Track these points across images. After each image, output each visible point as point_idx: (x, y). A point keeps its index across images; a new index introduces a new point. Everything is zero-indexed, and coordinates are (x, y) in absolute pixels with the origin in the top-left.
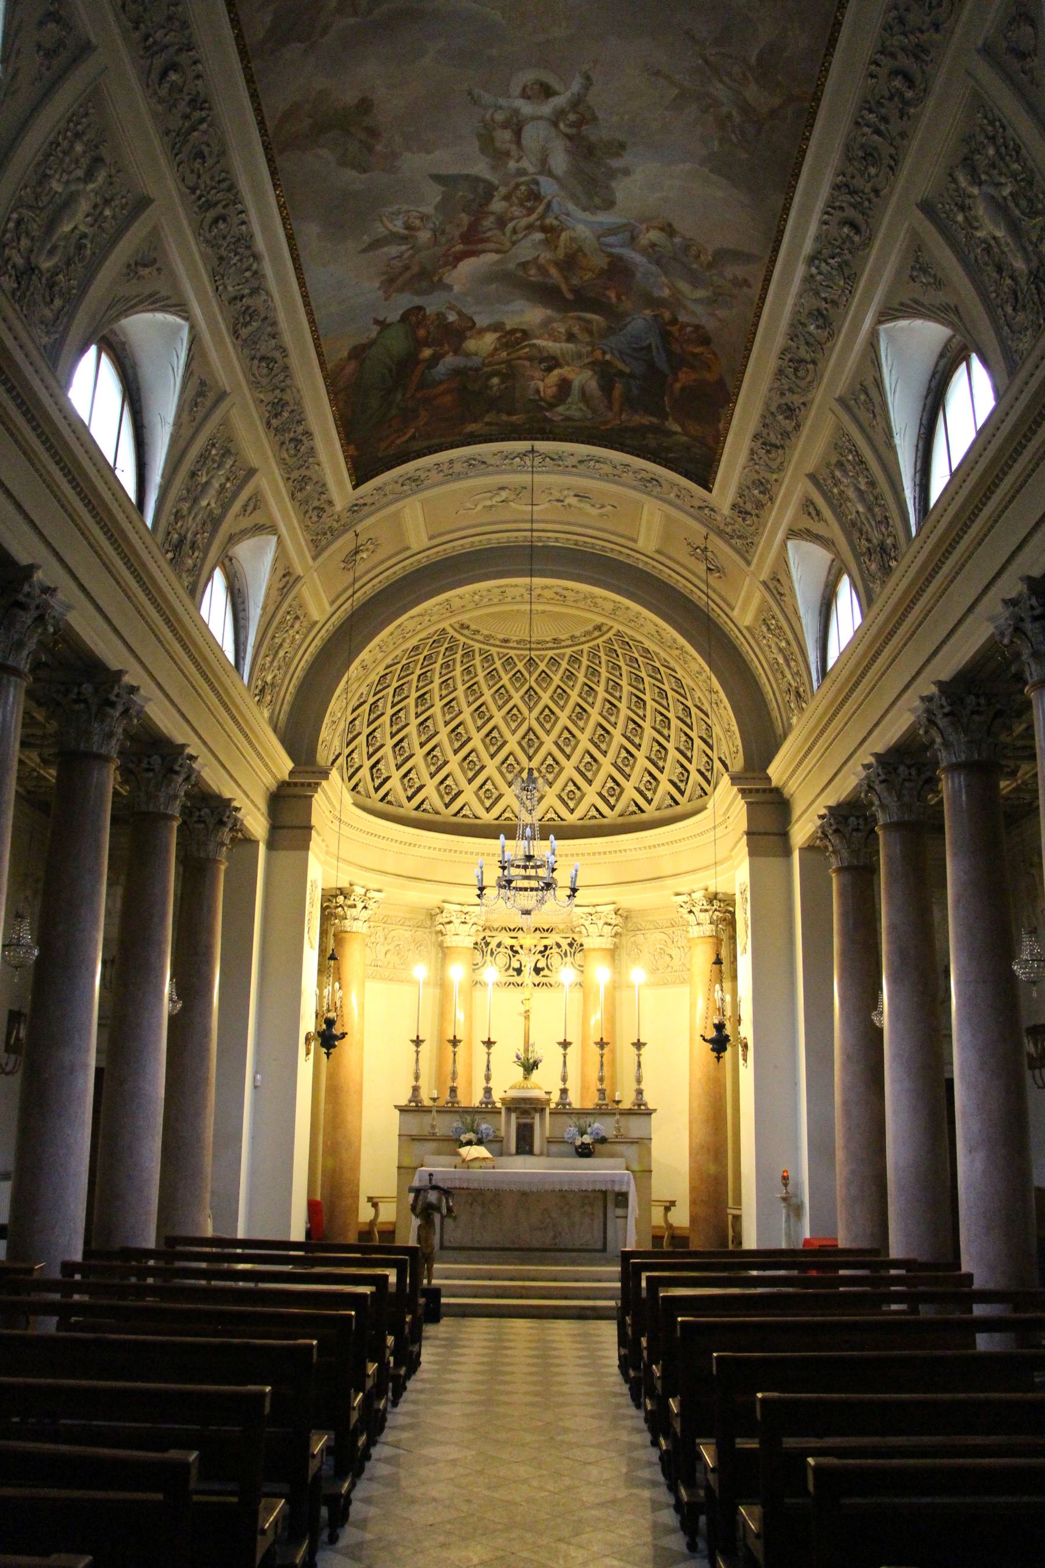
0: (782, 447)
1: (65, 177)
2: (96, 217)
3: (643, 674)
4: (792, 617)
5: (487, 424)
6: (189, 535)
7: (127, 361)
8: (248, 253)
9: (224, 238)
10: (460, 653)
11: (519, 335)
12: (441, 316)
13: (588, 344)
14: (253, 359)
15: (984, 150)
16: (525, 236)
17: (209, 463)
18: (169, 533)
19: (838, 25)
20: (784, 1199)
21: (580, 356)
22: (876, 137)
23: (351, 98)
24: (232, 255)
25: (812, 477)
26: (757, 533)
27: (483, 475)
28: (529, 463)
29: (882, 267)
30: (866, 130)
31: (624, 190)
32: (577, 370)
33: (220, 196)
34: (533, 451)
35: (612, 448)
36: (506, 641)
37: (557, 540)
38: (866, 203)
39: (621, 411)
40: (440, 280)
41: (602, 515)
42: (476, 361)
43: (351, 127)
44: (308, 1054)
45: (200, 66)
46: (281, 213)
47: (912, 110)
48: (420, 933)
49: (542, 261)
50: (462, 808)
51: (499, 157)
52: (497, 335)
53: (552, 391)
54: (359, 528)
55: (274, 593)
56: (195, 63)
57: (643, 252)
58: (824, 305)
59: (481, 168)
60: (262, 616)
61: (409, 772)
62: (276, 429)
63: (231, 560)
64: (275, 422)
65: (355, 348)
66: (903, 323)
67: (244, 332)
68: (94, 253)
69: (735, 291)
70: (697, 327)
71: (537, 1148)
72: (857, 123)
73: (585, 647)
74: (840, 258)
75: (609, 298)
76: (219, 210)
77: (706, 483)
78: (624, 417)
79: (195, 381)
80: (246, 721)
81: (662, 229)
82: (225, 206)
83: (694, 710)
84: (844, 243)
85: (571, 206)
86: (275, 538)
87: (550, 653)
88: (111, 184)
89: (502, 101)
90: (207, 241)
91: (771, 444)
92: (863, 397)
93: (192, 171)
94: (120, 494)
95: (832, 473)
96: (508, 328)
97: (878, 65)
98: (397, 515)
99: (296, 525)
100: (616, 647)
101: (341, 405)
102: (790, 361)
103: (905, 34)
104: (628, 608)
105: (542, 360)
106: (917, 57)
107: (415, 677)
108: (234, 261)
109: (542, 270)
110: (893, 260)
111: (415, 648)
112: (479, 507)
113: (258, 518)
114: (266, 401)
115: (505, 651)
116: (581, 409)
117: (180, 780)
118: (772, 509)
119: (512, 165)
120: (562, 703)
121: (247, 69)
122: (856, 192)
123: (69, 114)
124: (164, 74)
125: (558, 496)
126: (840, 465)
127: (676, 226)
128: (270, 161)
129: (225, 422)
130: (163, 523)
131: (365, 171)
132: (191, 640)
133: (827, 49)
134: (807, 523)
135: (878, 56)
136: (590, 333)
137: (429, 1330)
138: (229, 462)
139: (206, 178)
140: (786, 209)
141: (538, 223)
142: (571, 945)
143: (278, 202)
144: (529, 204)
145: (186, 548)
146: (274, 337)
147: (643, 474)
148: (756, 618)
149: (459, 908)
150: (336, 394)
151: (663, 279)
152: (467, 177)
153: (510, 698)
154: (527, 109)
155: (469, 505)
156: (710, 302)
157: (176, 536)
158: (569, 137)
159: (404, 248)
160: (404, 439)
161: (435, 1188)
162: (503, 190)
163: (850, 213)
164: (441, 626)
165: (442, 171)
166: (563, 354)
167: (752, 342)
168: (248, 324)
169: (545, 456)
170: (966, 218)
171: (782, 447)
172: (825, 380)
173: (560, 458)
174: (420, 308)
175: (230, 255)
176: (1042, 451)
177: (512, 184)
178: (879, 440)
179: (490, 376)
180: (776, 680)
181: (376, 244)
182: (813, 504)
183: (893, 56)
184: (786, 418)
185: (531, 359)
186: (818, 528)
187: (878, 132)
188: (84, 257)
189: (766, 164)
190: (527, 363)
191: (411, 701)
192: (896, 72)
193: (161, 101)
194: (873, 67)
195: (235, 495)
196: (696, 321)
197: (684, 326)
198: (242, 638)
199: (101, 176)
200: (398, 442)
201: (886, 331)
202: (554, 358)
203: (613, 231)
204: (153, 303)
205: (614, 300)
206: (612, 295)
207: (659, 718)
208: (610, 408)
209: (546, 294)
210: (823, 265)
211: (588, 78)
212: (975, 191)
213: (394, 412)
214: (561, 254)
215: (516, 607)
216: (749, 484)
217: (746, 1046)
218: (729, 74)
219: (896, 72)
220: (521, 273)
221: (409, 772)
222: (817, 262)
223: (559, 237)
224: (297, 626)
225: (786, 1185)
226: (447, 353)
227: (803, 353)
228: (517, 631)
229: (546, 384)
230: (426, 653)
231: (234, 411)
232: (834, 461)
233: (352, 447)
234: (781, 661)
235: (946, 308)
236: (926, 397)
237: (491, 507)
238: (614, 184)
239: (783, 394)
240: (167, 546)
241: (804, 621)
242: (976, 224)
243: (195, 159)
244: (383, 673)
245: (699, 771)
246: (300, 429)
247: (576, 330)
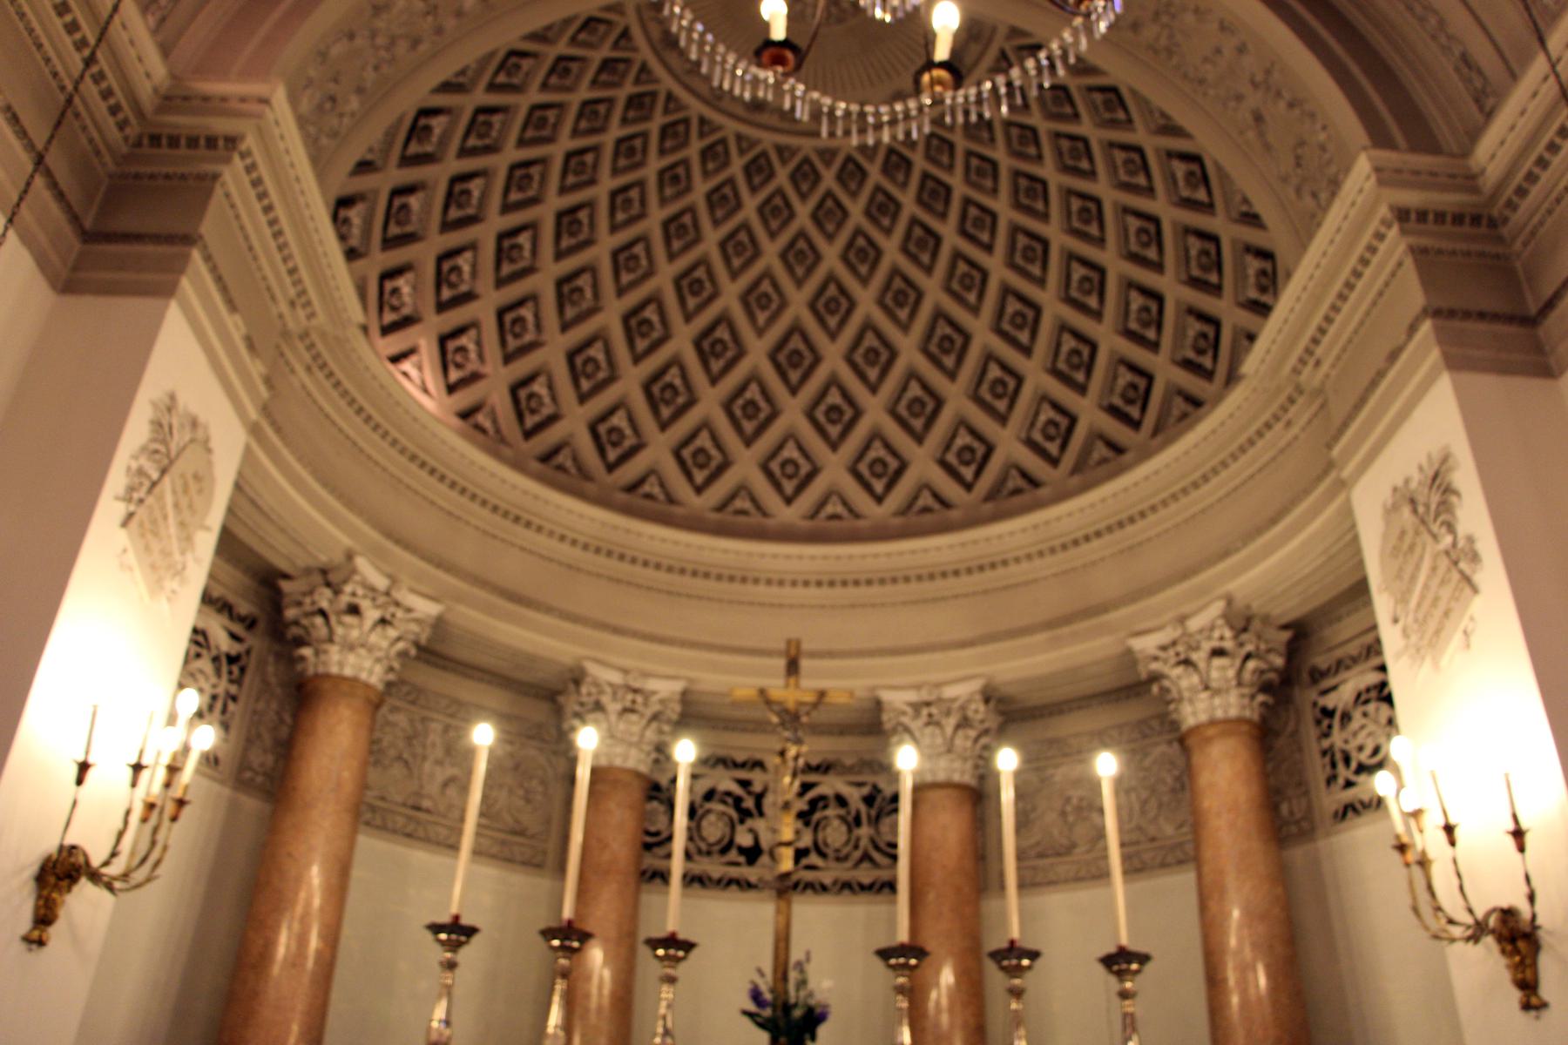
142: (869, 800)
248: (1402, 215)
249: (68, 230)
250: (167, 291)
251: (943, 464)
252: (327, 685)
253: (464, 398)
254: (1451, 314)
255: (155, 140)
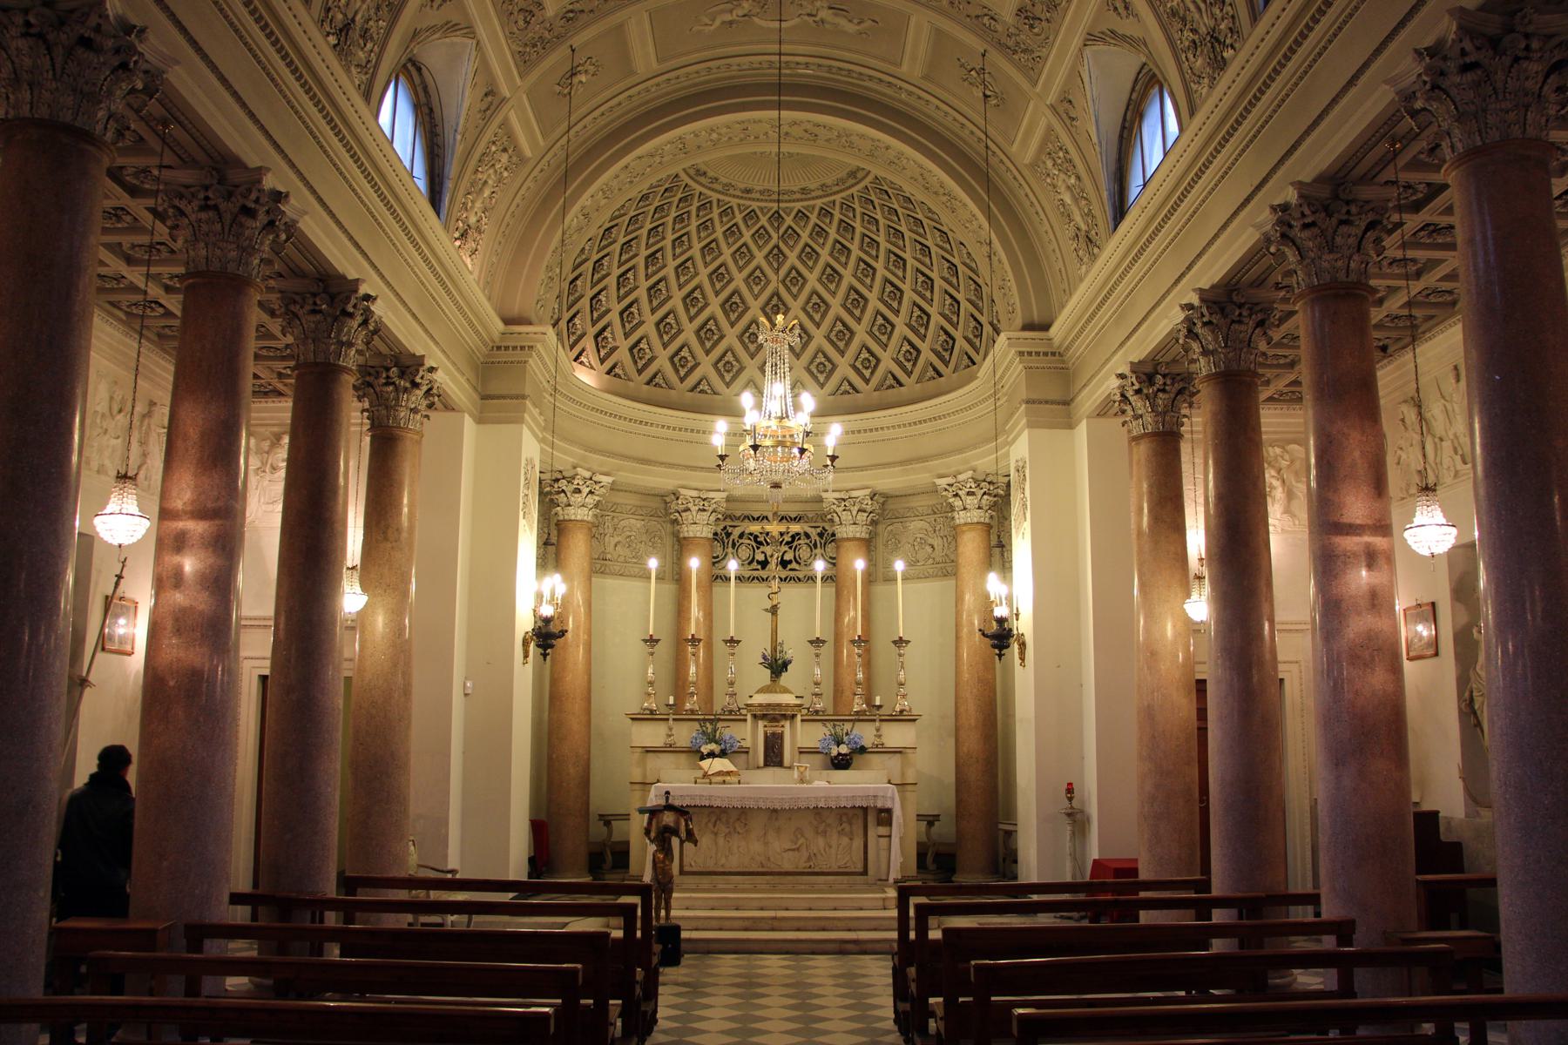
3: (903, 229)
20: (1069, 815)
26: (1046, 42)
36: (748, 191)
44: (526, 656)
48: (654, 524)
50: (699, 383)
54: (576, 41)
61: (639, 342)
71: (787, 762)
87: (798, 205)
98: (620, 27)
107: (644, 232)
111: (645, 197)
112: (718, 22)
117: (355, 323)
120: (810, 263)
132: (366, 154)
137: (668, 974)
142: (821, 535)
145: (355, 35)
149: (695, 494)
161: (669, 807)
164: (673, 171)
186: (1126, 27)
215: (759, 149)
217: (1023, 645)
221: (639, 342)
225: (1070, 799)
228: (762, 181)
230: (657, 204)
237: (731, 23)
244: (608, 225)
245: (966, 338)
248: (1021, 354)
249: (475, 396)
250: (519, 421)
251: (854, 367)
252: (571, 525)
253: (608, 364)
254: (1034, 402)
255: (499, 348)
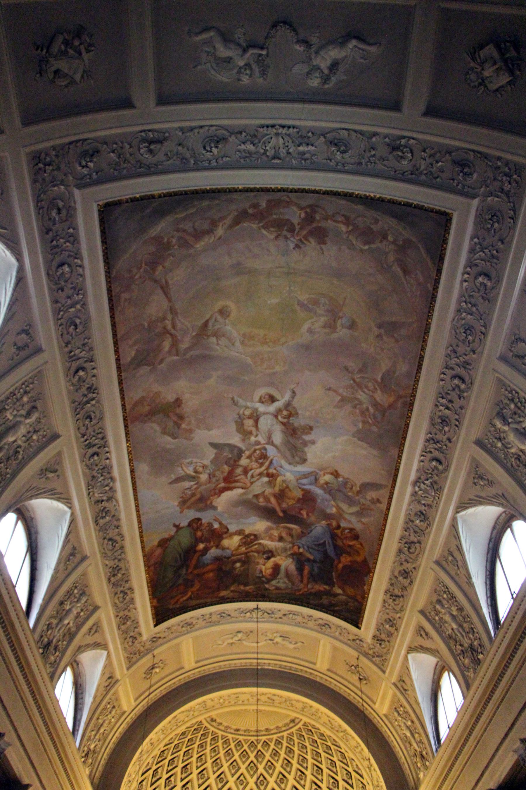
0: (402, 596)
1: (15, 412)
2: (28, 439)
3: (321, 751)
4: (414, 705)
5: (232, 591)
6: (55, 641)
7: (32, 530)
8: (108, 476)
9: (97, 465)
10: (210, 737)
11: (252, 537)
12: (210, 525)
13: (290, 542)
14: (104, 539)
15: (509, 408)
16: (258, 479)
17: (72, 597)
18: (42, 636)
19: (422, 358)
21: (285, 550)
22: (447, 411)
23: (170, 398)
24: (99, 475)
25: (422, 612)
26: (388, 652)
27: (229, 623)
28: (255, 616)
29: (456, 480)
30: (441, 408)
31: (311, 452)
32: (283, 558)
33: (97, 441)
34: (257, 608)
35: (302, 605)
36: (238, 730)
37: (269, 664)
38: (444, 447)
39: (308, 582)
40: (211, 503)
41: (295, 648)
42: (228, 553)
43: (170, 413)
45: (95, 371)
46: (129, 456)
47: (465, 394)
49: (266, 493)
51: (246, 434)
52: (240, 537)
53: (269, 571)
54: (156, 652)
55: (102, 689)
56: (93, 369)
57: (322, 487)
58: (423, 508)
59: (236, 440)
60: (92, 703)
62: (114, 584)
63: (78, 664)
64: (113, 579)
65: (162, 540)
66: (471, 510)
67: (102, 522)
68: (23, 458)
69: (373, 507)
70: (351, 530)
72: (436, 405)
73: (285, 734)
74: (432, 480)
75: (302, 514)
76: (95, 449)
77: (357, 624)
78: (310, 586)
79: (70, 546)
80: (72, 769)
81: (332, 474)
82: (69, 256)
83: (354, 774)
84: (433, 470)
85: (283, 463)
86: (105, 653)
88: (39, 422)
89: (249, 404)
90: (87, 466)
91: (396, 595)
92: (450, 558)
93: (84, 425)
94: (18, 606)
95: (435, 607)
96: (247, 532)
97: (445, 374)
98: (178, 645)
99: (119, 646)
100: (304, 734)
101: (151, 573)
102: (406, 543)
103: (457, 357)
104: (311, 707)
105: (264, 553)
106: (465, 368)
107: (182, 753)
108: (100, 480)
109: (267, 500)
110: (463, 474)
111: (183, 734)
112: (225, 644)
113: (97, 638)
114: (109, 565)
115: (237, 737)
116: (285, 583)
118: (397, 636)
119: (253, 439)
121: (119, 376)
122: (438, 442)
123: (24, 380)
124: (77, 371)
125: (271, 637)
126: (439, 602)
127: (340, 472)
128: (126, 426)
129: (84, 574)
130: (39, 630)
131: (175, 438)
132: (46, 709)
133: (417, 370)
134: (475, 491)
135: (445, 370)
136: (291, 536)
138: (84, 600)
139: (90, 430)
140: (400, 457)
141: (265, 472)
143: (128, 450)
144: (261, 461)
145: (51, 648)
146: (117, 528)
147: (320, 621)
148: (390, 708)
150: (149, 567)
151: (332, 502)
152: (229, 445)
153: (239, 768)
154: (262, 408)
155: (220, 642)
156: (359, 514)
157: (46, 640)
158: (283, 424)
159: (192, 483)
160: (185, 598)
162: (247, 453)
163: (436, 454)
164: (199, 719)
165: (216, 441)
166: (276, 548)
167: (382, 535)
168: (105, 517)
169: (264, 612)
170: (503, 444)
171: (402, 596)
172: (427, 552)
173: (273, 613)
174: (199, 519)
175: (98, 475)
176: (524, 656)
177: (253, 449)
178: (463, 581)
179: (235, 562)
180: (406, 748)
181: (178, 480)
182: (423, 629)
183: (452, 369)
184: (405, 578)
185: (258, 552)
186: (427, 644)
187: (448, 408)
188: (17, 459)
189: (387, 431)
190: (256, 554)
191: (178, 770)
192: (454, 377)
193: (73, 385)
194: (442, 376)
195: (83, 623)
196: (351, 526)
197: (345, 529)
198: (79, 717)
199: (35, 416)
200: (182, 600)
201: (461, 517)
202: (271, 551)
203: (306, 476)
204: (52, 494)
205: (305, 516)
206: (304, 513)
207: (332, 781)
208: (302, 581)
209: (268, 513)
210: (422, 485)
211: (294, 392)
212: (506, 428)
213: (181, 581)
214: (277, 489)
215: (244, 708)
216: (383, 622)
218: (367, 387)
219: (454, 377)
220: (255, 501)
222: (418, 484)
223: (276, 480)
224: (113, 712)
226: (212, 547)
227: (413, 538)
229: (266, 567)
231: (90, 568)
232: (434, 600)
233: (155, 601)
234: (408, 734)
235: (496, 496)
236: (487, 554)
237: (232, 644)
238: (306, 449)
239: (401, 564)
240: (39, 644)
241: (422, 706)
242: (510, 446)
243: (86, 418)
244: (162, 749)
246: (127, 585)
247: (284, 535)
